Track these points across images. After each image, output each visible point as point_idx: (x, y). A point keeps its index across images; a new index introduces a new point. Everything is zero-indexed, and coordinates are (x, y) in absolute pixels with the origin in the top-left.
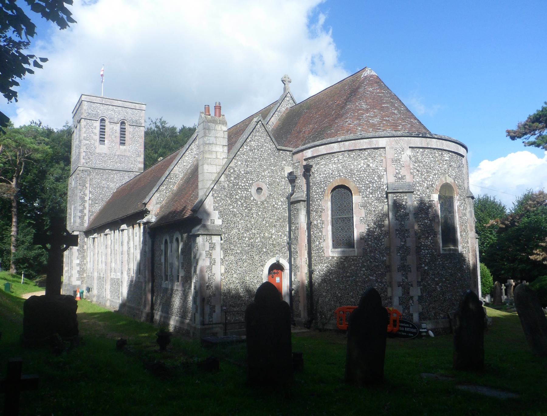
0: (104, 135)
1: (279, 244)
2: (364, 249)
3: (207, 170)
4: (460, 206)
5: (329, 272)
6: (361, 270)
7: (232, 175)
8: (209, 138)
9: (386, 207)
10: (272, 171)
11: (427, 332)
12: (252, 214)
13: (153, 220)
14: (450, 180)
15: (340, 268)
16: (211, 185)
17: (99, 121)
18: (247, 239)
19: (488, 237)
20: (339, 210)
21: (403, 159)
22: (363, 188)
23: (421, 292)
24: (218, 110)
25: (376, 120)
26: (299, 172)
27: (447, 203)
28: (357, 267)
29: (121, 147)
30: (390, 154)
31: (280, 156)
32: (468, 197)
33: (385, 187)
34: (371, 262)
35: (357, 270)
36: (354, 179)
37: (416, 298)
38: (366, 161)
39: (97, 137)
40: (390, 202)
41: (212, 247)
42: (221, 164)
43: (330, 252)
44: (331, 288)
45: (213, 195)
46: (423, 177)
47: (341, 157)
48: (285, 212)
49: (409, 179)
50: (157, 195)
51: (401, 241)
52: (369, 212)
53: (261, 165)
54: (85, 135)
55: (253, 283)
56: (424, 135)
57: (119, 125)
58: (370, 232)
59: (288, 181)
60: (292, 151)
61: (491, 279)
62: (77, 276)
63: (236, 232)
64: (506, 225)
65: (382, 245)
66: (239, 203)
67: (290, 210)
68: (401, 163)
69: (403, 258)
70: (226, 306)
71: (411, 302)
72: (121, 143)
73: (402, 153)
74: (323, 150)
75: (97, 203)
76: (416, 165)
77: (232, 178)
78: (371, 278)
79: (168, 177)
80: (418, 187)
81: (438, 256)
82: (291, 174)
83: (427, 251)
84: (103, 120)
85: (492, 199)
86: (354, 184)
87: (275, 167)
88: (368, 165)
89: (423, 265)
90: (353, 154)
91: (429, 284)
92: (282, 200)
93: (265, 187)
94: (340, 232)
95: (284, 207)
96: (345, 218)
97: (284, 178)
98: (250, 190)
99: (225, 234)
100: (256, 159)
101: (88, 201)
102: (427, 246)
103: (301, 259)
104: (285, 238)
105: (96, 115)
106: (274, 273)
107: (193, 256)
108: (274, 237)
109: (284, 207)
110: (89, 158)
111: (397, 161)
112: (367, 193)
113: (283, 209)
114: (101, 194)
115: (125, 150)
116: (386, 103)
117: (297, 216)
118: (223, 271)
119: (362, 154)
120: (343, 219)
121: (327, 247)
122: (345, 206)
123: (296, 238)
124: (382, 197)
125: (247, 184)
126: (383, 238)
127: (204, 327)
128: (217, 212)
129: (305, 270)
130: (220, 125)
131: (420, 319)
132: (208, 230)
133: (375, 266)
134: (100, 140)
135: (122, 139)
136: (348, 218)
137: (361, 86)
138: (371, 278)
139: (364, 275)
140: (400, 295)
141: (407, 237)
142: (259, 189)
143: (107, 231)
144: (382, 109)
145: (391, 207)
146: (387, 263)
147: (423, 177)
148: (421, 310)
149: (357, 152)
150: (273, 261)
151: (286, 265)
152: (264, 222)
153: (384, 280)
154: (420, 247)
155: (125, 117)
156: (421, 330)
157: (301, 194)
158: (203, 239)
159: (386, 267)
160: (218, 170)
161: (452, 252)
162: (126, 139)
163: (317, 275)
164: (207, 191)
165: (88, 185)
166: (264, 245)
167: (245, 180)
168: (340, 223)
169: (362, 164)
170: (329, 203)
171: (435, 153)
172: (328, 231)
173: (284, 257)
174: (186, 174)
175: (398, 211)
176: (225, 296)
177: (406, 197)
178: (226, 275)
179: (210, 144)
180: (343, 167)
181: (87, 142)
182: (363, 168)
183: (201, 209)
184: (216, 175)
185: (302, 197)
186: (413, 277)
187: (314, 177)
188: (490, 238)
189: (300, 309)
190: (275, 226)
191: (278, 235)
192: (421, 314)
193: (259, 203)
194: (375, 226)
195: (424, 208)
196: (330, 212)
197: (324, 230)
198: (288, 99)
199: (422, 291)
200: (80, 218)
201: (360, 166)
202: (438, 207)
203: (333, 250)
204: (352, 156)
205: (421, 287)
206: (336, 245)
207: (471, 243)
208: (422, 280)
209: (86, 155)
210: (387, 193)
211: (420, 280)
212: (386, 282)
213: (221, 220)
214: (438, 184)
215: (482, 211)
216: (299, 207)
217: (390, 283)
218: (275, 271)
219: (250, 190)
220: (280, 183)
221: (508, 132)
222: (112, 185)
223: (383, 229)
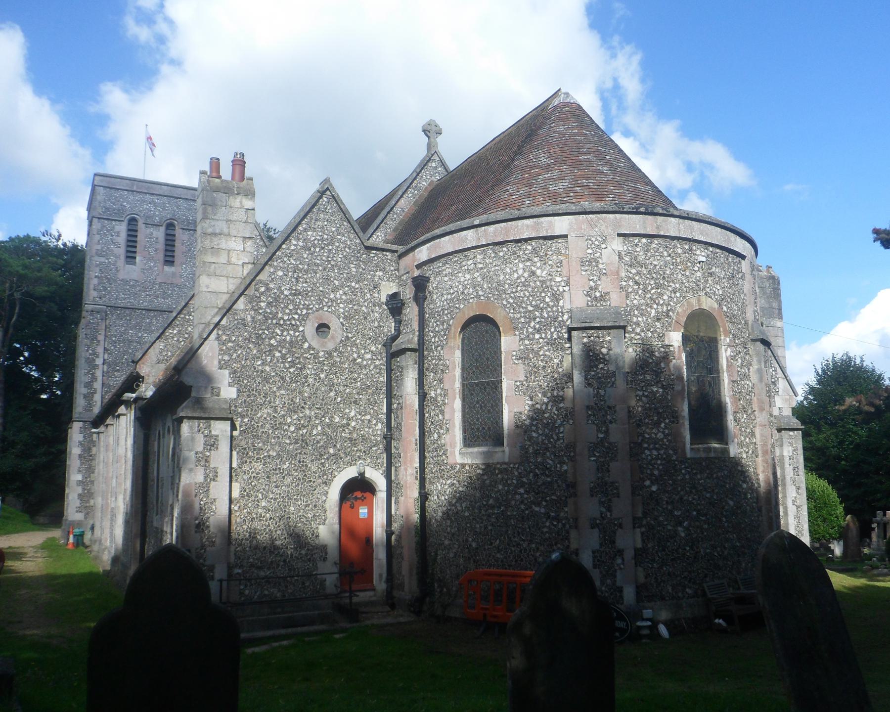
0: (136, 247)
1: (364, 439)
2: (523, 448)
3: (207, 287)
4: (734, 358)
5: (455, 496)
6: (516, 493)
7: (263, 298)
8: (213, 223)
9: (568, 360)
10: (354, 291)
11: (654, 627)
12: (306, 377)
13: (149, 394)
14: (708, 304)
15: (475, 488)
16: (214, 316)
18: (292, 428)
19: (850, 430)
20: (477, 368)
21: (604, 259)
22: (522, 320)
23: (643, 541)
24: (238, 168)
25: (562, 185)
26: (408, 293)
27: (704, 352)
28: (509, 485)
29: (167, 268)
30: (576, 248)
31: (370, 260)
32: (753, 340)
33: (565, 317)
34: (536, 475)
35: (508, 492)
36: (505, 302)
37: (629, 554)
38: (528, 263)
39: (121, 251)
40: (577, 349)
41: (212, 444)
42: (239, 275)
43: (459, 455)
44: (459, 530)
45: (218, 338)
46: (648, 296)
47: (479, 257)
48: (379, 373)
49: (616, 300)
50: (160, 345)
51: (599, 431)
52: (534, 371)
54: (99, 247)
55: (304, 520)
56: (650, 210)
58: (537, 415)
59: (387, 312)
60: (396, 252)
61: (840, 509)
62: (78, 503)
63: (269, 414)
64: (877, 408)
65: (559, 439)
66: (278, 354)
67: (389, 371)
68: (601, 266)
69: (603, 468)
70: (241, 567)
71: (619, 561)
73: (603, 246)
74: (447, 244)
75: (118, 370)
77: (263, 304)
78: (537, 509)
79: (184, 312)
80: (637, 316)
81: (682, 462)
82: (394, 296)
83: (655, 453)
85: (858, 362)
86: (503, 313)
87: (358, 282)
88: (533, 273)
89: (648, 483)
90: (503, 251)
92: (373, 348)
93: (335, 324)
94: (478, 412)
95: (377, 363)
96: (488, 383)
97: (380, 306)
98: (301, 329)
99: (243, 417)
100: (318, 265)
101: (101, 367)
102: (656, 441)
103: (406, 469)
104: (379, 426)
105: (121, 211)
106: (356, 498)
108: (353, 424)
109: (377, 363)
110: (105, 289)
111: (591, 263)
112: (530, 330)
113: (375, 367)
114: (125, 352)
115: (174, 274)
116: (589, 153)
117: (400, 380)
119: (520, 249)
120: (483, 386)
121: (453, 445)
122: (488, 359)
123: (399, 427)
124: (559, 337)
125: (296, 317)
128: (226, 372)
129: (414, 493)
130: (239, 198)
131: (639, 597)
132: (203, 409)
133: (544, 484)
134: (127, 257)
135: (169, 253)
136: (493, 383)
137: (543, 124)
138: (537, 509)
139: (522, 502)
140: (597, 546)
141: (611, 422)
142: (323, 328)
143: (108, 421)
144: (578, 164)
145: (578, 361)
147: (648, 296)
148: (642, 579)
150: (350, 473)
152: (332, 394)
153: (562, 514)
154: (640, 444)
155: (174, 215)
156: (639, 624)
157: (410, 338)
158: (191, 428)
159: (568, 486)
160: (232, 287)
161: (712, 455)
162: (176, 254)
164: (204, 330)
165: (101, 338)
166: (331, 441)
167: (291, 307)
168: (478, 395)
169: (520, 270)
170: (458, 354)
172: (453, 411)
173: (376, 466)
175: (591, 367)
176: (240, 545)
177: (608, 339)
178: (243, 502)
179: (215, 234)
180: (483, 279)
181: (103, 259)
182: (523, 280)
183: (189, 365)
184: (225, 297)
185: (409, 341)
186: (622, 508)
188: (855, 433)
189: (403, 573)
190: (355, 402)
191: (363, 421)
192: (640, 589)
193: (321, 354)
194: (546, 400)
195: (651, 363)
196: (458, 372)
197: (447, 410)
198: (434, 165)
199: (645, 538)
200: (85, 396)
201: (516, 276)
202: (680, 360)
203: (465, 450)
204: (501, 254)
205: (643, 529)
206: (469, 440)
207: (762, 435)
208: (645, 514)
209: (99, 284)
210: (570, 330)
211: (640, 515)
212: (566, 518)
214: (681, 311)
215: (839, 384)
216: (404, 364)
217: (576, 520)
218: (358, 494)
219: (301, 329)
220: (368, 314)
221: (876, 232)
223: (562, 405)
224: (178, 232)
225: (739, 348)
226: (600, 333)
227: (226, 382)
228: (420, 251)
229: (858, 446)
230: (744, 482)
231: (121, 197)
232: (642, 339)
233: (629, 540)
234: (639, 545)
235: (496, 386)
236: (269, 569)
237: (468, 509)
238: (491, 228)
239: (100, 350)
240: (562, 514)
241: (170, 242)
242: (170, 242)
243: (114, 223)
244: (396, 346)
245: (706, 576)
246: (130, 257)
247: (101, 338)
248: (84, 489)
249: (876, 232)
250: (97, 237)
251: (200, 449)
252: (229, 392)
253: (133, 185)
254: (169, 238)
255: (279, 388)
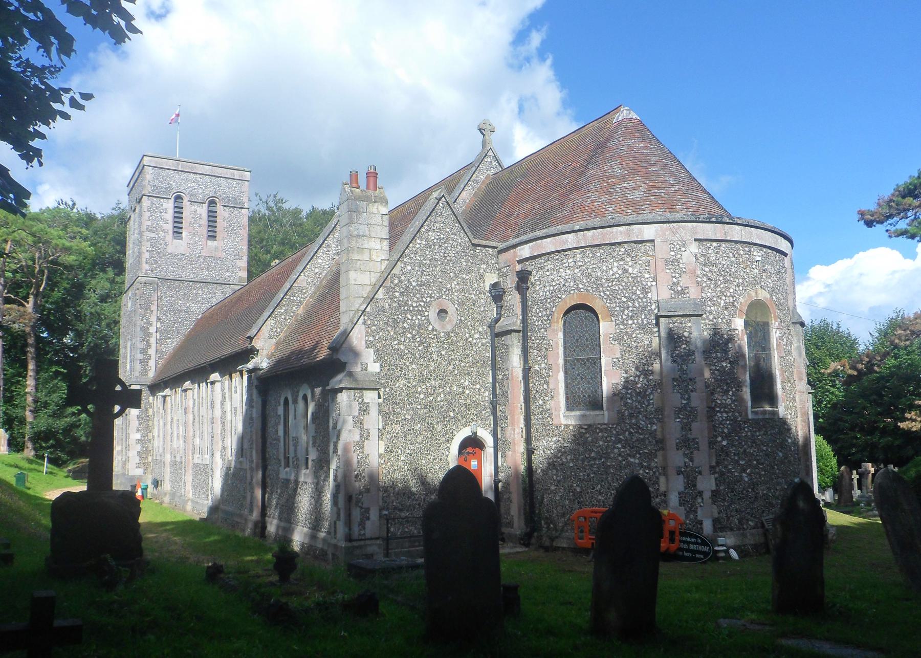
2: (619, 412)
3: (355, 280)
4: (781, 338)
5: (560, 451)
6: (615, 448)
7: (397, 289)
9: (656, 341)
10: (464, 281)
12: (431, 354)
14: (763, 295)
17: (173, 199)
18: (422, 396)
20: (577, 347)
23: (717, 485)
24: (372, 179)
25: (638, 195)
26: (510, 283)
30: (662, 251)
33: (653, 307)
34: (631, 433)
36: (602, 294)
37: (707, 495)
38: (622, 263)
39: (169, 227)
45: (364, 323)
46: (718, 289)
49: (694, 293)
50: (271, 322)
52: (627, 350)
53: (444, 272)
54: (149, 223)
57: (205, 206)
58: (628, 384)
59: (490, 299)
61: (834, 461)
62: (137, 460)
65: (649, 404)
66: (409, 335)
67: (494, 348)
68: (681, 266)
69: (686, 427)
70: (388, 509)
71: (700, 500)
72: (209, 236)
73: (683, 249)
74: (549, 245)
76: (707, 269)
77: (397, 294)
78: (632, 460)
79: (289, 293)
80: (710, 306)
81: (745, 422)
82: (495, 286)
83: (725, 415)
84: (178, 198)
85: (76, 83)
88: (626, 271)
89: (719, 439)
90: (599, 252)
91: (729, 471)
92: (481, 329)
93: (451, 309)
94: (579, 383)
95: (484, 341)
96: (588, 360)
97: (485, 294)
98: (426, 314)
99: (385, 387)
101: (154, 335)
103: (514, 430)
104: (487, 394)
106: (469, 453)
107: (331, 425)
108: (467, 392)
109: (484, 341)
110: (156, 262)
111: (673, 263)
112: (625, 317)
115: (216, 248)
117: (506, 356)
118: (382, 450)
119: (614, 251)
120: (583, 362)
121: (558, 409)
123: (505, 394)
125: (422, 304)
126: (651, 393)
127: (350, 544)
129: (521, 448)
133: (637, 440)
134: (175, 232)
138: (632, 460)
141: (692, 391)
142: (442, 312)
145: (664, 341)
146: (659, 436)
147: (718, 289)
149: (607, 248)
150: (466, 432)
151: (489, 440)
152: (451, 367)
153: (653, 464)
154: (713, 409)
156: (716, 548)
157: (515, 321)
158: (349, 397)
159: (657, 442)
160: (373, 280)
161: (767, 416)
163: (539, 459)
164: (354, 316)
165: (154, 308)
167: (418, 296)
169: (615, 268)
171: (738, 249)
172: (557, 381)
173: (485, 427)
174: (319, 288)
175: (676, 347)
177: (689, 324)
180: (583, 274)
181: (153, 235)
185: (514, 324)
186: (702, 458)
187: (535, 291)
188: (833, 393)
189: (512, 514)
190: (468, 374)
192: (716, 521)
193: (442, 334)
195: (719, 343)
196: (561, 350)
197: (551, 380)
198: (489, 160)
201: (611, 272)
202: (743, 341)
203: (568, 413)
204: (598, 254)
205: (717, 475)
207: (801, 400)
208: (718, 463)
209: (151, 257)
210: (658, 318)
211: (714, 464)
212: (656, 467)
213: (378, 365)
214: (743, 302)
215: (817, 347)
216: (510, 342)
217: (664, 468)
218: (470, 449)
219: (426, 314)
221: (862, 214)
222: (194, 307)
223: (651, 377)
224: (219, 208)
225: (785, 330)
226: (683, 319)
227: (372, 359)
228: (523, 249)
229: (835, 406)
230: (790, 437)
231: (168, 176)
232: (715, 325)
233: (707, 484)
234: (714, 488)
235: (596, 362)
236: (408, 511)
237: (572, 460)
238: (590, 233)
239: (153, 319)
240: (653, 464)
241: (212, 217)
242: (212, 217)
243: (162, 200)
244: (499, 327)
245: (763, 512)
246: (177, 232)
247: (154, 308)
248: (143, 447)
249: (862, 214)
250: (147, 214)
251: (356, 414)
252: (374, 368)
253: (178, 165)
254: (211, 214)
255: (411, 363)
